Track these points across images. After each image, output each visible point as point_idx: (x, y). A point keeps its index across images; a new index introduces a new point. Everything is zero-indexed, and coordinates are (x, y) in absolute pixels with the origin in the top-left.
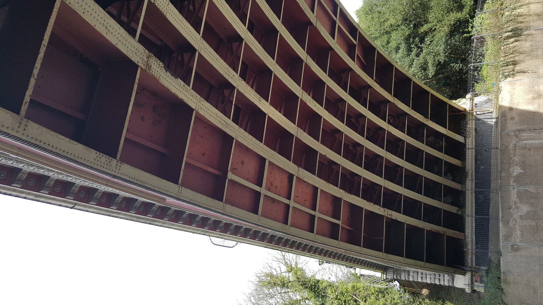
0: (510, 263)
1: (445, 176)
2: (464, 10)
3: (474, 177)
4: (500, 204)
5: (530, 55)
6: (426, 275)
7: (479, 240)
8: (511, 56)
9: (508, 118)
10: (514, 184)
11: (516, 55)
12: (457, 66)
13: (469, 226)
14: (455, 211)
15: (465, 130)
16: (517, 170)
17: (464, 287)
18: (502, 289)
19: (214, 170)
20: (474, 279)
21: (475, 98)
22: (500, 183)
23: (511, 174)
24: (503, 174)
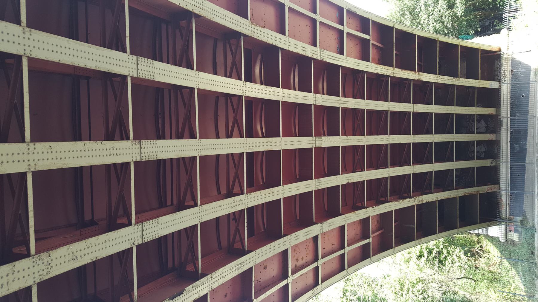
1: (478, 123)
3: (509, 126)
7: (513, 124)
17: (499, 236)
18: (536, 264)
20: (509, 228)
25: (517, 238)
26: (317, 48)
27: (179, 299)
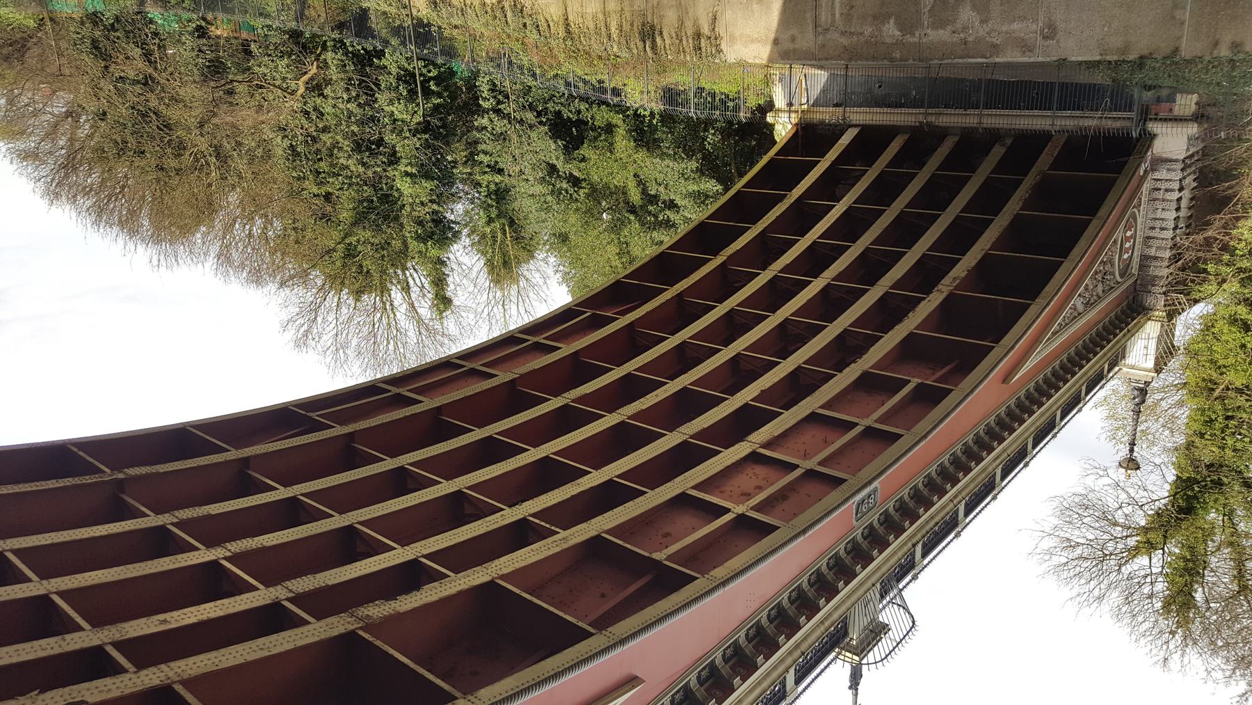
0: (1081, 41)
2: (614, 121)
4: (956, 61)
5: (686, 9)
6: (1156, 219)
8: (684, 42)
9: (791, 46)
10: (917, 34)
11: (683, 34)
12: (712, 138)
13: (1001, 122)
14: (1003, 150)
15: (836, 126)
16: (891, 31)
18: (1141, 57)
19: (638, 582)
20: (1162, 115)
21: (777, 106)
22: (914, 60)
23: (897, 40)
24: (897, 55)
25: (1190, 96)
26: (850, 481)
27: (555, 667)
